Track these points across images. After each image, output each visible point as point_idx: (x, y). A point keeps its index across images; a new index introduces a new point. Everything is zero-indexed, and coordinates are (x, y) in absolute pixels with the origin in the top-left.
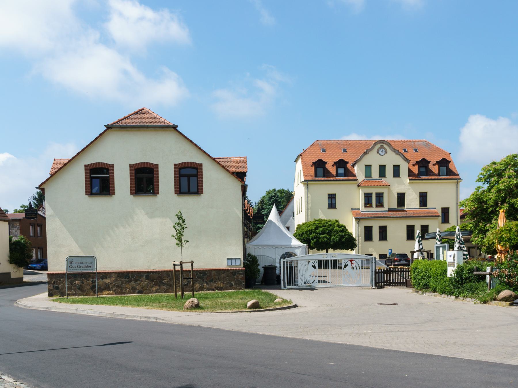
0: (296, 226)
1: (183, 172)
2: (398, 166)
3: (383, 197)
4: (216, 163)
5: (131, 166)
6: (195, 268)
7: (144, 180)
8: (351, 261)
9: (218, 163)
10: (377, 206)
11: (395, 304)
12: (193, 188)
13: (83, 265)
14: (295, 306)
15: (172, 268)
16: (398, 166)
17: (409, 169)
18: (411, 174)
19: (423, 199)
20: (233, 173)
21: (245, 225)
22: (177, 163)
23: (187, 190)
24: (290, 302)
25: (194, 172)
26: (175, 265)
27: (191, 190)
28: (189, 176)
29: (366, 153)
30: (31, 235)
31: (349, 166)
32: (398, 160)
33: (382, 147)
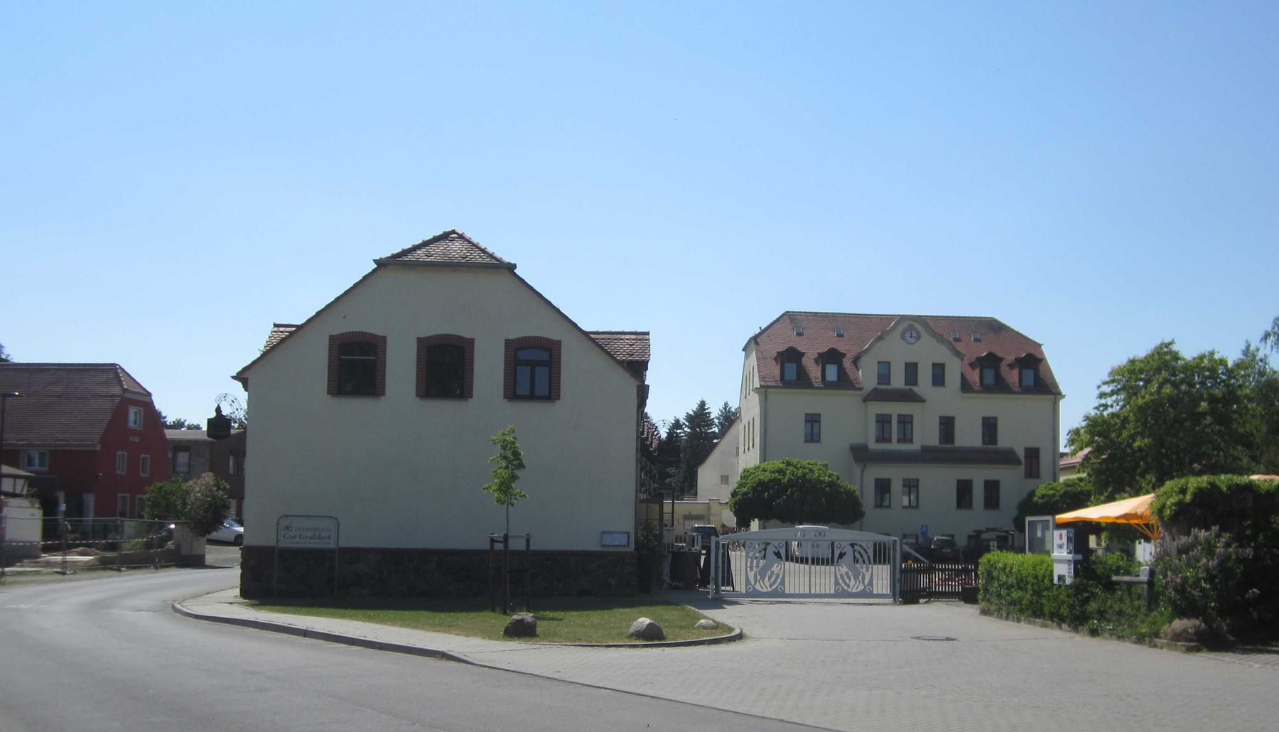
0: (741, 470)
1: (523, 355)
2: (942, 366)
3: (911, 422)
4: (590, 343)
5: (420, 340)
6: (532, 548)
7: (445, 368)
8: (852, 545)
9: (593, 340)
10: (899, 441)
11: (948, 639)
12: (541, 388)
13: (310, 534)
14: (740, 637)
15: (488, 547)
16: (942, 366)
17: (963, 376)
18: (966, 387)
19: (990, 426)
20: (621, 363)
21: (642, 468)
22: (511, 337)
23: (527, 393)
24: (731, 629)
25: (544, 356)
26: (493, 541)
27: (537, 393)
28: (533, 365)
29: (880, 338)
30: (231, 472)
31: (847, 363)
32: (941, 354)
33: (911, 328)
